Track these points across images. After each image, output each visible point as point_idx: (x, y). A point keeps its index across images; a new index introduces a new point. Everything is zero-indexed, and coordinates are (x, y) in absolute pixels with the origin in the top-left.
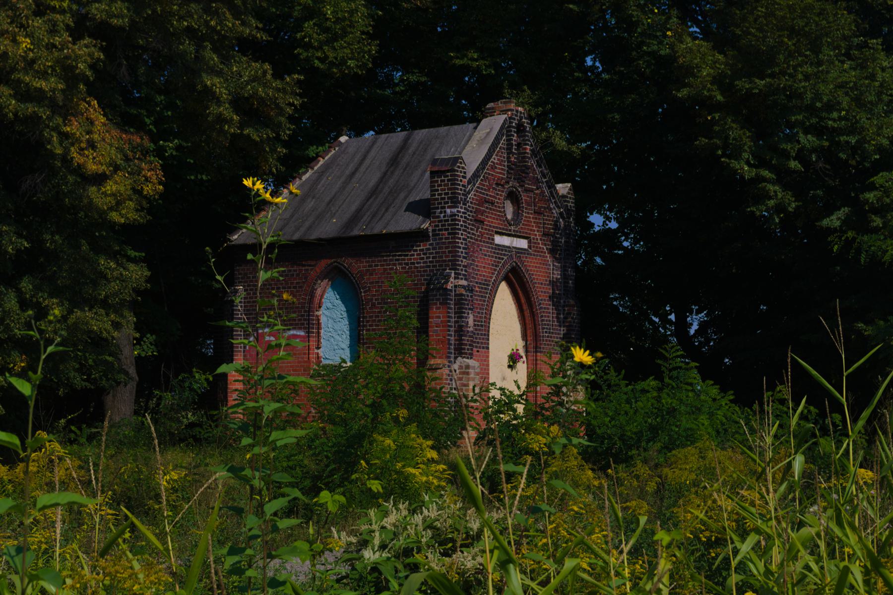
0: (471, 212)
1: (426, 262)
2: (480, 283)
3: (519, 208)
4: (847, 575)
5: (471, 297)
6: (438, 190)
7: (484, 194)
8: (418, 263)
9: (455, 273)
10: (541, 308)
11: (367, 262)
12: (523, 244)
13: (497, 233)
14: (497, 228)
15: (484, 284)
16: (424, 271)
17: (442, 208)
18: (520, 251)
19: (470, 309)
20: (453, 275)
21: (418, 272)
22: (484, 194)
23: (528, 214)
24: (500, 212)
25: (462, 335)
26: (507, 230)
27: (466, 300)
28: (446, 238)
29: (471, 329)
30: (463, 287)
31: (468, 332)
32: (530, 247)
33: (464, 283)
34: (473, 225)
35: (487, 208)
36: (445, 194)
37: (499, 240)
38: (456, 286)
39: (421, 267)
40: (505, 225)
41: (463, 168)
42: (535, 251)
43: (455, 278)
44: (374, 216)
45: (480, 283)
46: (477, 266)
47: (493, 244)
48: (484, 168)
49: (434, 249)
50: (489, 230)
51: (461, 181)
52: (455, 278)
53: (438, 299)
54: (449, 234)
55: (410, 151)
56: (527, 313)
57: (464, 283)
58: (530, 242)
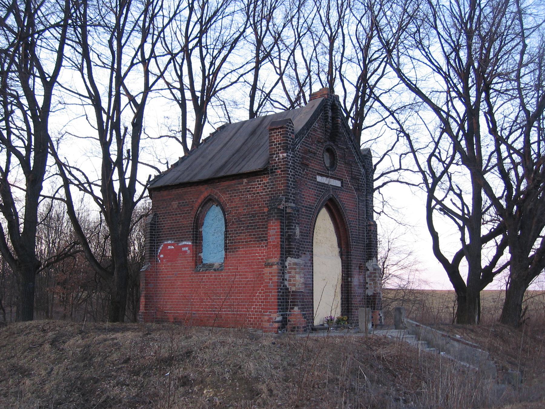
0: (298, 157)
1: (267, 192)
2: (306, 207)
3: (334, 159)
4: (83, 51)
5: (298, 215)
6: (274, 142)
7: (308, 147)
8: (261, 192)
9: (286, 198)
10: (351, 226)
11: (229, 194)
12: (338, 183)
13: (319, 174)
14: (318, 170)
15: (309, 208)
16: (265, 198)
17: (277, 154)
18: (335, 188)
19: (297, 223)
20: (284, 199)
21: (262, 198)
22: (308, 147)
23: (340, 164)
24: (320, 160)
25: (290, 242)
26: (325, 173)
27: (294, 217)
28: (280, 174)
29: (298, 237)
30: (292, 208)
31: (295, 239)
32: (342, 186)
33: (293, 205)
34: (300, 167)
35: (311, 157)
36: (279, 144)
37: (319, 179)
38: (286, 207)
39: (263, 195)
40: (324, 170)
41: (291, 127)
42: (346, 189)
43: (286, 202)
44: (235, 164)
45: (306, 207)
46: (303, 195)
47: (316, 181)
48: (308, 130)
49: (272, 182)
50: (312, 172)
51: (290, 135)
52: (286, 202)
53: (274, 216)
54: (281, 171)
55: (264, 126)
56: (341, 230)
57: (293, 205)
58: (342, 183)
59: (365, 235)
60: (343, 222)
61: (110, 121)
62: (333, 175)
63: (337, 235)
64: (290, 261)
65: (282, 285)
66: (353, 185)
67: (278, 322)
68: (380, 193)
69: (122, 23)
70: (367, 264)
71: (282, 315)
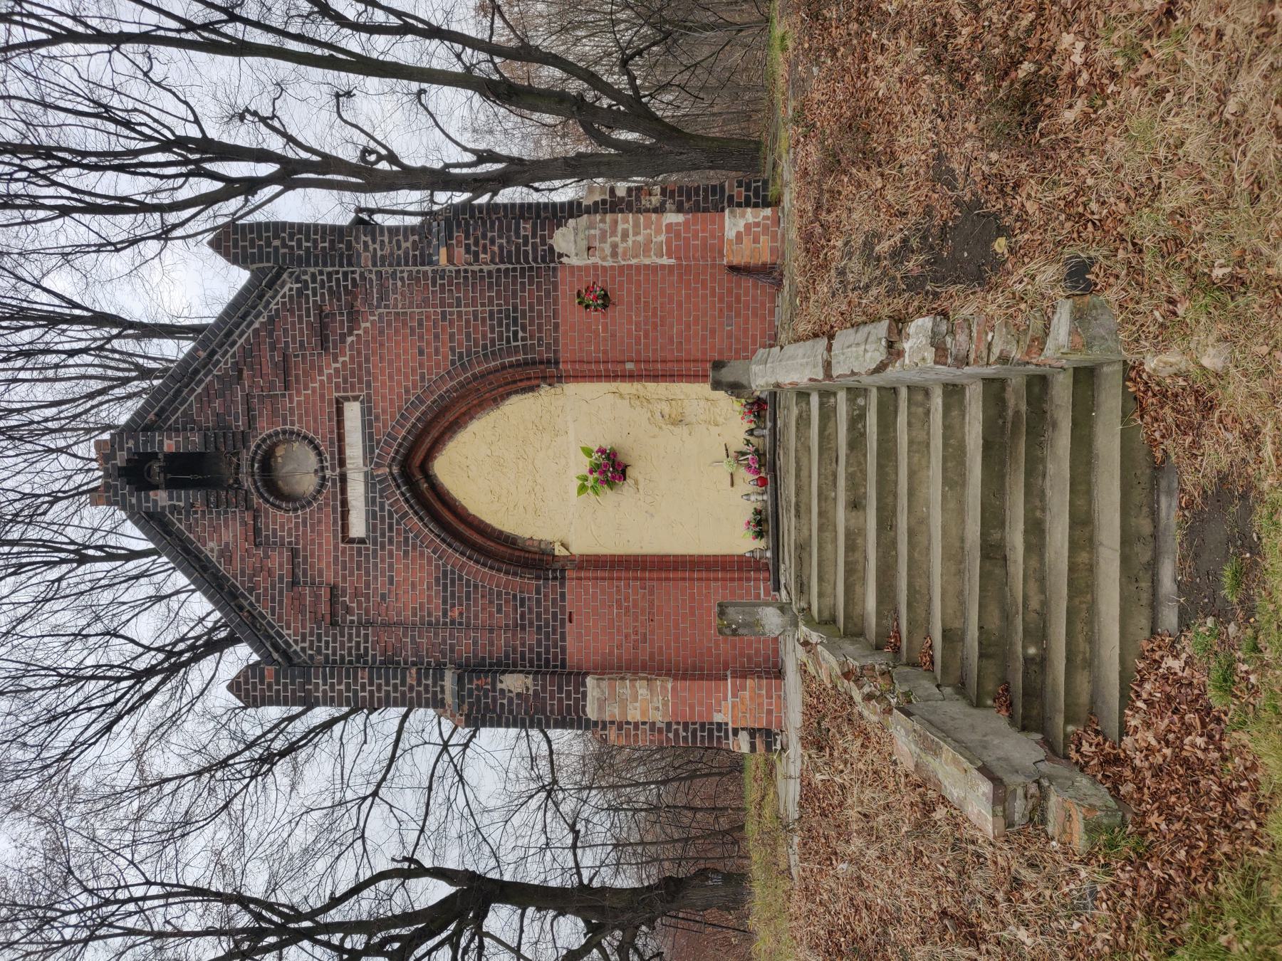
15: (445, 590)
32: (356, 398)
58: (347, 399)
62: (332, 458)
66: (343, 341)
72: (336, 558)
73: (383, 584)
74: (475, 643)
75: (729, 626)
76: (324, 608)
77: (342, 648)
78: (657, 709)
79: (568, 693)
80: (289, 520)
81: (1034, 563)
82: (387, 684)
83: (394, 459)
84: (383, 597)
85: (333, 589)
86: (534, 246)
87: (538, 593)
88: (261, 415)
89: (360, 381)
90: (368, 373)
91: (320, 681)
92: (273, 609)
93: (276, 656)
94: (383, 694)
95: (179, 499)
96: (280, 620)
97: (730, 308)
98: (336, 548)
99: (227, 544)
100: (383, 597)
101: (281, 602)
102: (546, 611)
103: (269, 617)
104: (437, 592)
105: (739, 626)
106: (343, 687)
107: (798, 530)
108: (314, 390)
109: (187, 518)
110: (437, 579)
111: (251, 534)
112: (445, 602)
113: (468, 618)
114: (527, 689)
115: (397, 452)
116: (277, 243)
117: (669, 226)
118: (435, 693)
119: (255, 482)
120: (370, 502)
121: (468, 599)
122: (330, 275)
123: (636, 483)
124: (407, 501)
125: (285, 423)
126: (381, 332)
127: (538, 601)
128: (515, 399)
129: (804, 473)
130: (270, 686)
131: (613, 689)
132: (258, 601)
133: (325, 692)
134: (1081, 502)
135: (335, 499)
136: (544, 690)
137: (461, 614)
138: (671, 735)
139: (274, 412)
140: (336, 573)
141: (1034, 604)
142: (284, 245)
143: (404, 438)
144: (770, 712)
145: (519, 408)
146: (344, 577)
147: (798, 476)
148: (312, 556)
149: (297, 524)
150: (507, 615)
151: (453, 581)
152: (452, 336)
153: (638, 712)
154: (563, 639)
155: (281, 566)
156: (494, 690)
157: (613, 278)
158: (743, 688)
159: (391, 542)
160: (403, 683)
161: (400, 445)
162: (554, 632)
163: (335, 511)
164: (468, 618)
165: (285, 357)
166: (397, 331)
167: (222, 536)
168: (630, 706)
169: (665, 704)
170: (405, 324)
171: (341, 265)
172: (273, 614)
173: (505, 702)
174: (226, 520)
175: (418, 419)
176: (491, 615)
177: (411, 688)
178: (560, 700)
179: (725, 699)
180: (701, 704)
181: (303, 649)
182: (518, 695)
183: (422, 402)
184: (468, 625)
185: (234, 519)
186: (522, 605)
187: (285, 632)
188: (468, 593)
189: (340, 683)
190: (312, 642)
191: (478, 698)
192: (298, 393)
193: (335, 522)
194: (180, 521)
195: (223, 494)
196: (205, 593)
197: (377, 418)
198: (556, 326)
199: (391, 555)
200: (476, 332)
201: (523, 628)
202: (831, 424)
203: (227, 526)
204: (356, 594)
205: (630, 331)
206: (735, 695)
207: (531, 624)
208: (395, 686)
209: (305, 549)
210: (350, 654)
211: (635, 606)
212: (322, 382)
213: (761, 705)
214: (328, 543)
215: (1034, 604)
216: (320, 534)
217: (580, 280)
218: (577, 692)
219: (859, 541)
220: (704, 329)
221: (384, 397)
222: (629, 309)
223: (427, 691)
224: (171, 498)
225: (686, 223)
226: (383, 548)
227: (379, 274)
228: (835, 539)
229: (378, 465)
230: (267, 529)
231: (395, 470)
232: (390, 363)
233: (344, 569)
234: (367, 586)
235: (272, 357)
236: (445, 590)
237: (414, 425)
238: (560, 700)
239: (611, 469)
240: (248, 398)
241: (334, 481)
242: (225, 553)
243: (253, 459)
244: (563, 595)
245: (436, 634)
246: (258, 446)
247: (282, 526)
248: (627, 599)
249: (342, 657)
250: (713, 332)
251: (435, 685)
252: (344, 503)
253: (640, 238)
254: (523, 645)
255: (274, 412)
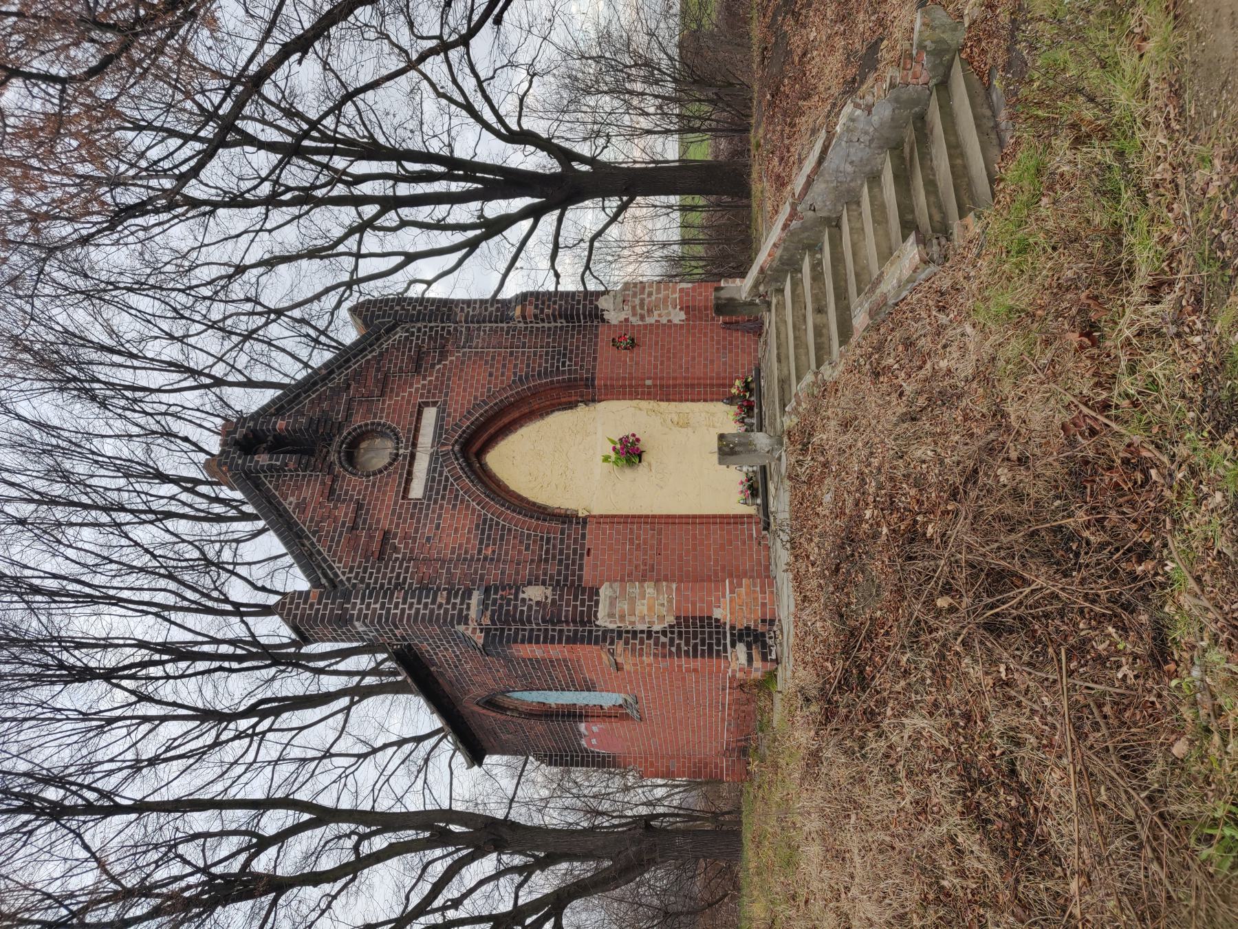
12: (430, 415)
15: (483, 533)
22: (341, 533)
32: (434, 404)
58: (427, 404)
59: (546, 325)
60: (517, 401)
61: (478, 232)
62: (407, 441)
63: (548, 414)
64: (603, 620)
65: (663, 639)
66: (433, 366)
67: (750, 659)
68: (493, 77)
69: (191, 713)
70: (614, 322)
71: (733, 645)
72: (394, 510)
73: (430, 529)
74: (503, 573)
75: (728, 445)
76: (375, 546)
77: (384, 578)
78: (663, 605)
79: (583, 601)
80: (361, 483)
81: (932, 199)
82: (419, 602)
83: (456, 441)
84: (428, 539)
85: (386, 535)
86: (585, 306)
87: (563, 533)
88: (357, 412)
89: (441, 392)
90: (448, 386)
91: (358, 601)
92: (330, 547)
93: (323, 581)
94: (413, 612)
95: (277, 460)
96: (335, 555)
97: (724, 348)
98: (396, 503)
99: (305, 499)
100: (428, 539)
101: (339, 541)
102: (568, 547)
103: (325, 554)
104: (476, 535)
105: (736, 445)
106: (378, 606)
107: (780, 370)
108: (403, 397)
109: (277, 480)
110: (477, 526)
111: (327, 491)
112: (481, 543)
113: (500, 554)
114: (546, 598)
115: (460, 436)
116: (398, 308)
117: (681, 290)
118: (461, 610)
119: (340, 458)
120: (431, 470)
121: (502, 539)
122: (431, 328)
123: (650, 465)
124: (462, 469)
125: (375, 417)
126: (463, 363)
127: (562, 540)
128: (556, 414)
129: (783, 336)
130: (312, 605)
131: (623, 590)
132: (319, 541)
133: (360, 610)
134: (952, 139)
135: (403, 469)
136: (561, 598)
137: (494, 552)
138: (674, 649)
139: (369, 411)
140: (391, 522)
141: (937, 217)
142: (403, 308)
143: (468, 427)
144: (764, 605)
145: (559, 420)
146: (398, 525)
147: (778, 337)
148: (374, 509)
149: (367, 487)
150: (533, 552)
151: (490, 526)
152: (515, 366)
153: (645, 608)
154: (581, 569)
155: (346, 515)
156: (516, 599)
157: (639, 331)
158: (740, 585)
159: (443, 498)
160: (433, 602)
161: (464, 432)
162: (574, 564)
163: (401, 475)
164: (500, 554)
165: (386, 377)
166: (475, 362)
167: (302, 494)
168: (638, 603)
169: (670, 601)
170: (481, 358)
171: (442, 322)
172: (329, 551)
173: (525, 608)
174: (309, 481)
175: (481, 415)
176: (520, 552)
177: (440, 606)
178: (575, 607)
179: (724, 596)
180: (702, 601)
181: (349, 579)
182: (538, 603)
183: (486, 404)
184: (499, 560)
185: (316, 480)
186: (548, 543)
187: (335, 566)
188: (502, 535)
189: (375, 603)
190: (358, 573)
191: (501, 606)
192: (391, 398)
193: (400, 484)
194: (270, 482)
195: (313, 460)
196: (276, 531)
197: (449, 415)
198: (595, 359)
199: (441, 507)
200: (534, 362)
201: (546, 560)
202: (800, 287)
203: (308, 485)
204: (406, 536)
205: (649, 362)
206: (732, 592)
207: (554, 558)
208: (426, 605)
209: (369, 504)
210: (389, 583)
211: (645, 543)
212: (411, 393)
213: (756, 599)
214: (390, 500)
215: (937, 217)
216: (384, 494)
217: (615, 332)
218: (590, 600)
219: (824, 331)
220: (706, 359)
221: (457, 402)
222: (650, 347)
223: (454, 608)
224: (271, 459)
225: (694, 289)
226: (436, 502)
227: (468, 329)
228: (807, 353)
229: (444, 445)
230: (341, 489)
231: (457, 448)
232: (466, 381)
233: (399, 518)
234: (416, 531)
235: (376, 376)
236: (483, 533)
237: (477, 419)
238: (575, 607)
239: (630, 452)
240: (350, 401)
241: (405, 457)
242: (302, 506)
243: (343, 442)
244: (583, 536)
245: (470, 566)
246: (349, 434)
247: (354, 487)
248: (638, 538)
249: (382, 585)
250: (712, 361)
251: (462, 604)
252: (410, 473)
253: (661, 296)
254: (545, 574)
255: (369, 411)
